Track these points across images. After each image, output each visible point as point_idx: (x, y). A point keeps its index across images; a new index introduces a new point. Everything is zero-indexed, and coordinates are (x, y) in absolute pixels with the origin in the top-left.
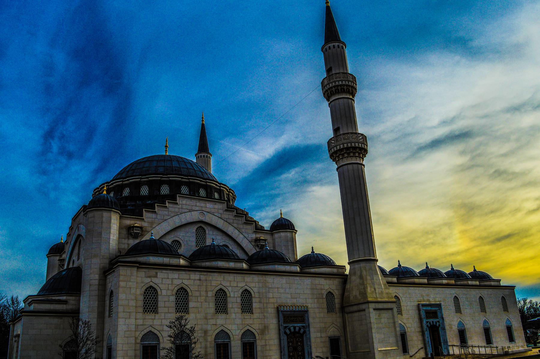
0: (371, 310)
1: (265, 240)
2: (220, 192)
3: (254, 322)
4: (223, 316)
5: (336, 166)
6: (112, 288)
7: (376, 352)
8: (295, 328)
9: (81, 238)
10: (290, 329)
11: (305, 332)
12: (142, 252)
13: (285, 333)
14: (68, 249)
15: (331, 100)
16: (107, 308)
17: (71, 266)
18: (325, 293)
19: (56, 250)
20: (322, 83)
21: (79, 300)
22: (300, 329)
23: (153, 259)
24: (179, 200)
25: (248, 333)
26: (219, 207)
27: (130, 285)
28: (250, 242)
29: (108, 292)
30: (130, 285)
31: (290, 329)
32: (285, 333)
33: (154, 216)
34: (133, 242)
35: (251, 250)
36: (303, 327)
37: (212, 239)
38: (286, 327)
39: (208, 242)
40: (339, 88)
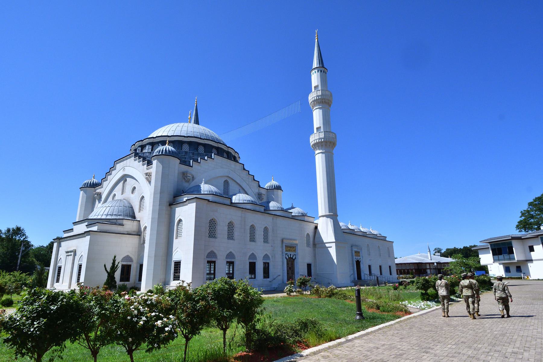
3: (232, 246)
11: (295, 258)
38: (286, 254)
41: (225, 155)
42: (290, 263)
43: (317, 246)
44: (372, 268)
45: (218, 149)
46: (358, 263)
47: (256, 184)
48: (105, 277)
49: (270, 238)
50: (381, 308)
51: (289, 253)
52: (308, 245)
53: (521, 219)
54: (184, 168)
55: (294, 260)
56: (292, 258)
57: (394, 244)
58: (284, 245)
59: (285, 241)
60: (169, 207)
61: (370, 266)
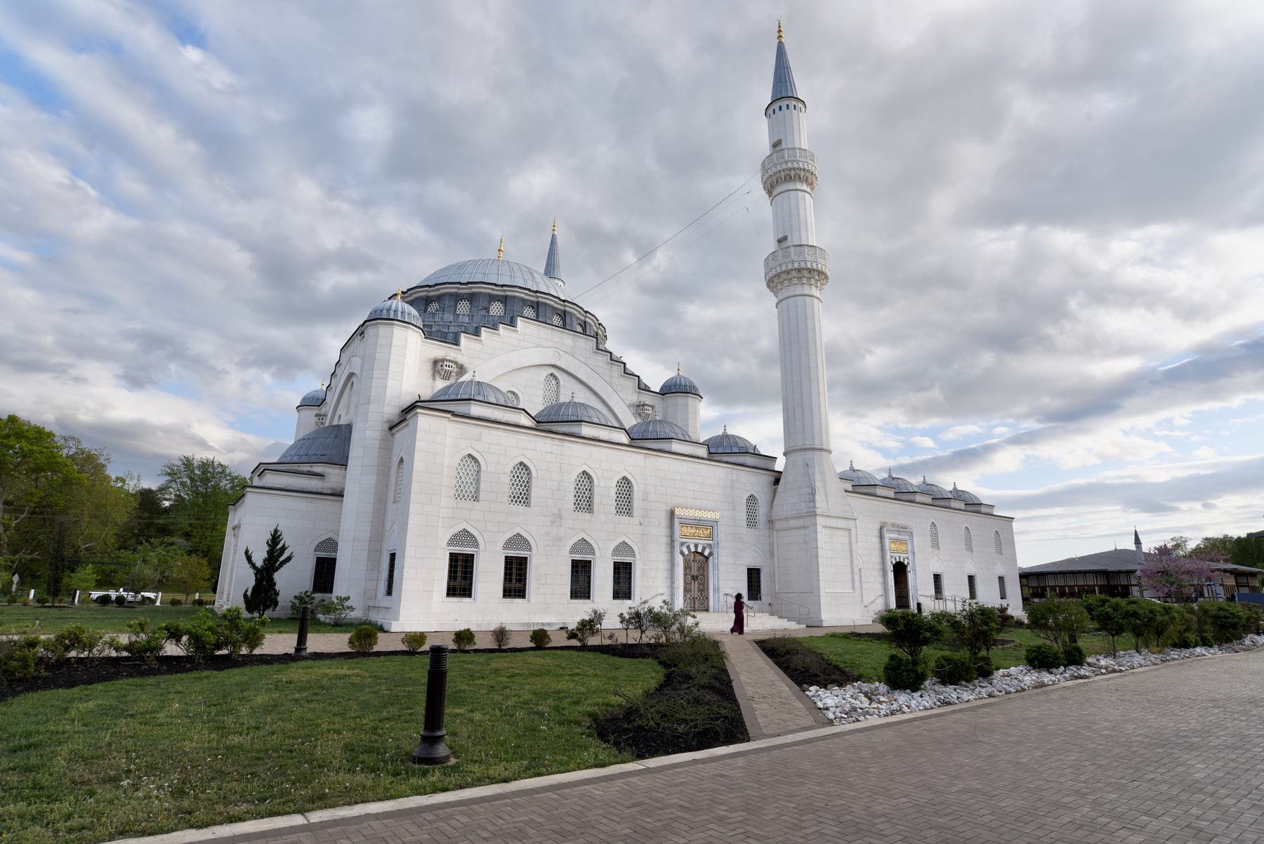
0: (819, 528)
1: (653, 407)
2: (584, 325)
3: (627, 531)
4: (587, 516)
5: (775, 300)
6: (403, 454)
7: (822, 594)
8: (696, 546)
9: (353, 379)
10: (688, 547)
11: (711, 554)
12: (454, 400)
13: (682, 553)
14: (331, 399)
15: (775, 193)
16: (392, 487)
17: (335, 423)
18: (376, 617)
19: (313, 402)
20: (763, 164)
21: (345, 477)
22: (704, 549)
23: (476, 410)
24: (520, 322)
25: (624, 547)
26: (587, 344)
27: (436, 439)
28: (629, 406)
29: (396, 460)
30: (436, 439)
31: (688, 547)
32: (682, 553)
33: (478, 346)
34: (440, 384)
35: (630, 421)
36: (710, 545)
37: (569, 392)
38: (682, 544)
39: (564, 399)
40: (793, 173)
41: (556, 320)
42: (695, 567)
43: (777, 525)
44: (945, 582)
45: (536, 306)
46: (900, 570)
47: (631, 384)
48: (250, 581)
49: (637, 504)
50: (497, 688)
51: (897, 555)
52: (752, 522)
53: (815, 292)
54: (439, 350)
55: (707, 558)
56: (702, 554)
57: (1016, 526)
58: (677, 522)
59: (677, 512)
60: (389, 433)
61: (937, 578)
